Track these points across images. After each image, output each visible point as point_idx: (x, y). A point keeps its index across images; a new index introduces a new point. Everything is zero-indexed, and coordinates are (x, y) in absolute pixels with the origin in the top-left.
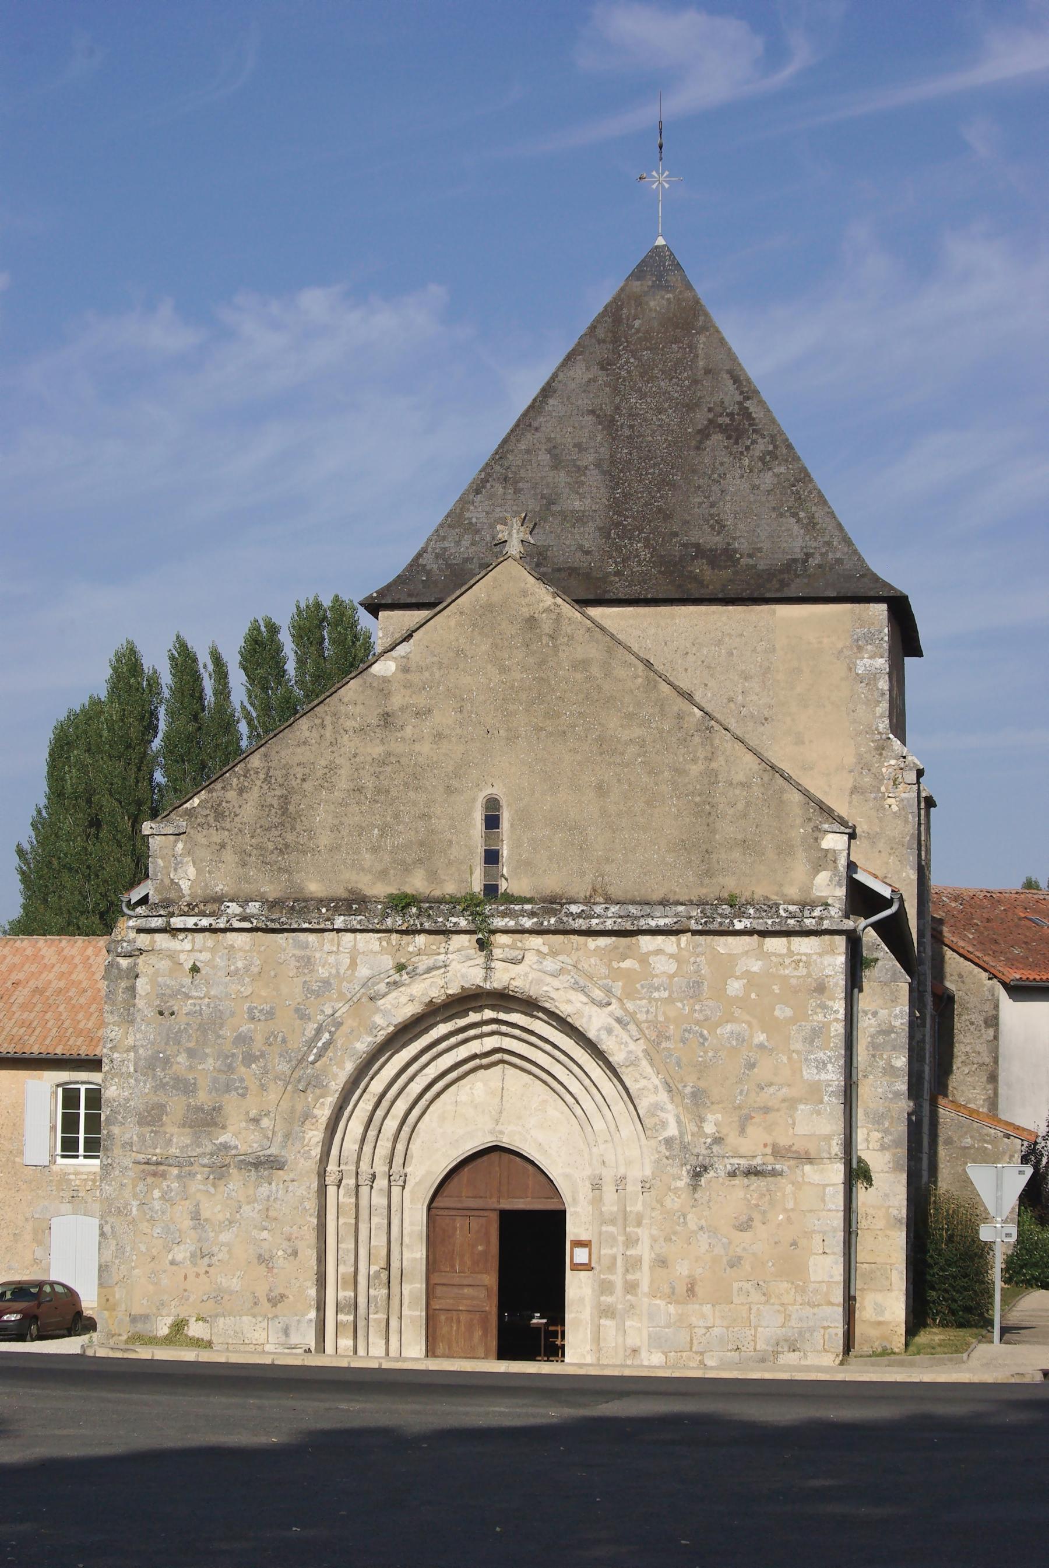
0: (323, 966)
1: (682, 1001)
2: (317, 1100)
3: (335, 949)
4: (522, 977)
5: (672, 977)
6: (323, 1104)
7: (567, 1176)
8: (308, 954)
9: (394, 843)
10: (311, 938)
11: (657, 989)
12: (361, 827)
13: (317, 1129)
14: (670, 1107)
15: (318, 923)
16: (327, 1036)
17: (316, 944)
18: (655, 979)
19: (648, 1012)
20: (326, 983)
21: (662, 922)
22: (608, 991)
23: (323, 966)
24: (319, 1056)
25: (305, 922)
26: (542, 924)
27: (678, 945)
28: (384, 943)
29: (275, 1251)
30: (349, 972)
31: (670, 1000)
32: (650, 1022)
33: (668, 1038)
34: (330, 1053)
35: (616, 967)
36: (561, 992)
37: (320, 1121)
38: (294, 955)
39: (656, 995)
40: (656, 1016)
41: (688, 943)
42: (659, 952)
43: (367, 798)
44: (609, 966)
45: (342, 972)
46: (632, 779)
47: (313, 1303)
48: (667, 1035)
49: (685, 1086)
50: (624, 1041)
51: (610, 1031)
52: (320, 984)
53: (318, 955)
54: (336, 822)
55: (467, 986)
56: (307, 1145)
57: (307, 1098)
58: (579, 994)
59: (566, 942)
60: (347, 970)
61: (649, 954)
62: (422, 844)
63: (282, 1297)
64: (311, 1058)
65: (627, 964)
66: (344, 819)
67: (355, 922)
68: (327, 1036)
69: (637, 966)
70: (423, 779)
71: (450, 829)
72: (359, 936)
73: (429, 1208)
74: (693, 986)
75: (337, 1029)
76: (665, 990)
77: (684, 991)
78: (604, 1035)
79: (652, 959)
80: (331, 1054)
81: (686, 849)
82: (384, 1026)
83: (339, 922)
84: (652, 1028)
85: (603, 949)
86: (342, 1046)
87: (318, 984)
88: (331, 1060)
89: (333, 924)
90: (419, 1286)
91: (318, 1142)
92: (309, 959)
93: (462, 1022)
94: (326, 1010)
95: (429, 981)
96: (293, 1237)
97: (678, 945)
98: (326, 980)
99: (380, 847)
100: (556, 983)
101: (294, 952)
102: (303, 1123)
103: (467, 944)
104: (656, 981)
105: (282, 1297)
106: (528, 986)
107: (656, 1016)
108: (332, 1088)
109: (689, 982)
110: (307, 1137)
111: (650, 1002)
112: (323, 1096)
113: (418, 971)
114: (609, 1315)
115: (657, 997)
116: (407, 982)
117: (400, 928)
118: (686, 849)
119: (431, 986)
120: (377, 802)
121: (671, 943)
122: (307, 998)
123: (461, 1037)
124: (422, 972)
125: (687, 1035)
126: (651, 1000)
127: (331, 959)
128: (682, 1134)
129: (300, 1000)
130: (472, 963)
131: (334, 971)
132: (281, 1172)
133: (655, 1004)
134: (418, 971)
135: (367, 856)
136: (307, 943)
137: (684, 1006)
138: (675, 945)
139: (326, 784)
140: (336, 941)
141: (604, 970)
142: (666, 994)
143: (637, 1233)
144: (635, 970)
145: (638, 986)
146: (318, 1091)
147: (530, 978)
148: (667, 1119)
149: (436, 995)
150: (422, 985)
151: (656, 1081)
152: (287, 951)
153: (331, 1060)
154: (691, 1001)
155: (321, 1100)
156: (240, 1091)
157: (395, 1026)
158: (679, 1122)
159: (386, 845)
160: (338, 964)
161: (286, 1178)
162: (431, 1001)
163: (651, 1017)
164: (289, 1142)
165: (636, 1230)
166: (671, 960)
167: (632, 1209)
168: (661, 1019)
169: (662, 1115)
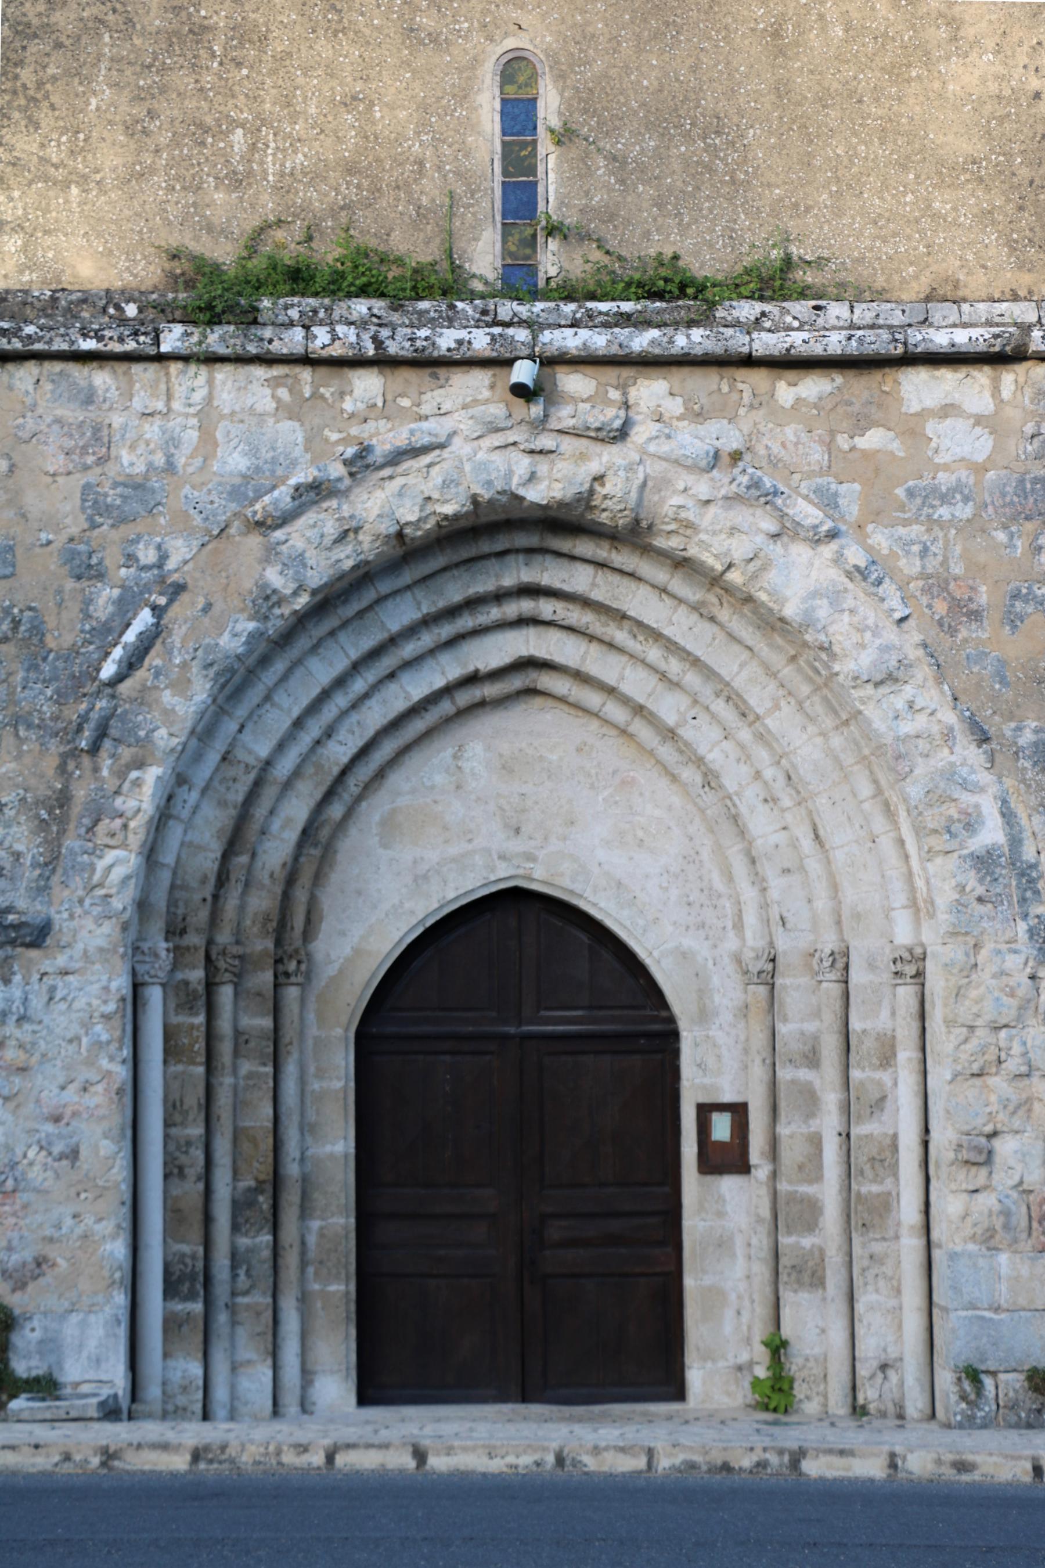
0: (132, 447)
1: (1005, 527)
2: (121, 774)
3: (160, 405)
4: (622, 473)
5: (980, 469)
6: (137, 783)
7: (684, 955)
8: (92, 415)
9: (282, 165)
10: (102, 378)
11: (945, 499)
12: (200, 125)
13: (124, 845)
14: (984, 777)
15: (121, 340)
16: (144, 619)
17: (113, 394)
18: (940, 475)
19: (924, 552)
20: (137, 486)
21: (961, 338)
22: (829, 502)
23: (132, 447)
24: (131, 664)
25: (85, 336)
26: (671, 342)
27: (996, 390)
28: (283, 393)
29: (19, 1152)
30: (198, 461)
31: (974, 527)
32: (929, 577)
33: (975, 615)
34: (154, 659)
35: (846, 447)
36: (713, 510)
37: (132, 824)
38: (58, 421)
39: (944, 512)
40: (945, 562)
41: (1019, 388)
42: (948, 410)
43: (213, 55)
44: (830, 446)
45: (181, 461)
46: (854, 14)
47: (117, 1275)
48: (973, 606)
49: (1019, 729)
50: (870, 622)
51: (835, 598)
52: (128, 491)
53: (117, 420)
54: (139, 111)
55: (486, 494)
56: (100, 885)
57: (96, 770)
58: (759, 512)
59: (725, 388)
60: (192, 457)
61: (923, 415)
62: (351, 169)
63: (39, 1265)
64: (108, 671)
65: (873, 439)
66: (161, 105)
67: (216, 339)
68: (144, 619)
69: (896, 446)
70: (350, 9)
71: (418, 133)
72: (223, 374)
73: (361, 1037)
74: (1033, 490)
75: (171, 601)
76: (966, 499)
77: (1012, 503)
78: (823, 611)
79: (931, 428)
80: (158, 662)
81: (981, 180)
82: (288, 591)
83: (172, 339)
84: (935, 590)
85: (815, 406)
86: (184, 641)
87: (119, 490)
88: (157, 675)
89: (157, 342)
90: (342, 1221)
91: (128, 877)
92: (97, 430)
93: (455, 592)
94: (141, 555)
95: (399, 481)
96: (68, 1112)
97: (996, 390)
98: (139, 480)
99: (250, 173)
100: (702, 488)
101: (59, 412)
102: (90, 830)
103: (486, 394)
104: (944, 479)
105: (39, 1265)
106: (634, 495)
107: (945, 562)
108: (161, 744)
109: (1022, 481)
110: (101, 865)
111: (929, 530)
112: (140, 764)
113: (370, 459)
114: (806, 1279)
115: (947, 517)
116: (342, 486)
117: (324, 353)
118: (981, 180)
119: (400, 494)
120: (239, 65)
121: (977, 389)
122: (94, 526)
123: (446, 630)
124: (380, 460)
125: (1019, 605)
126: (932, 523)
127: (152, 430)
128: (1015, 842)
129: (74, 530)
130: (498, 439)
131: (159, 460)
132: (33, 953)
133: (941, 534)
134: (370, 459)
135: (219, 196)
136: (91, 389)
137: (1011, 536)
138: (987, 394)
139: (111, 17)
140: (163, 387)
141: (817, 455)
142: (965, 511)
143: (880, 1084)
144: (892, 453)
145: (900, 492)
146: (126, 753)
147: (641, 476)
148: (977, 806)
149: (412, 518)
150: (380, 496)
151: (949, 717)
152: (40, 411)
153: (157, 675)
154: (1029, 526)
155: (134, 774)
156: (524, 372)
157: (314, 593)
158: (1008, 815)
159: (265, 172)
160: (172, 442)
161: (47, 966)
162: (400, 535)
163: (932, 564)
164: (56, 879)
165: (878, 1075)
166: (978, 430)
167: (868, 1025)
168: (957, 569)
169: (967, 799)
